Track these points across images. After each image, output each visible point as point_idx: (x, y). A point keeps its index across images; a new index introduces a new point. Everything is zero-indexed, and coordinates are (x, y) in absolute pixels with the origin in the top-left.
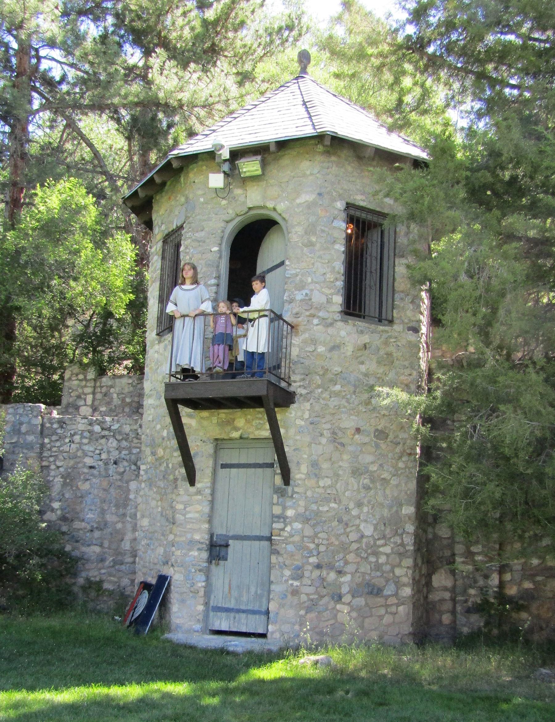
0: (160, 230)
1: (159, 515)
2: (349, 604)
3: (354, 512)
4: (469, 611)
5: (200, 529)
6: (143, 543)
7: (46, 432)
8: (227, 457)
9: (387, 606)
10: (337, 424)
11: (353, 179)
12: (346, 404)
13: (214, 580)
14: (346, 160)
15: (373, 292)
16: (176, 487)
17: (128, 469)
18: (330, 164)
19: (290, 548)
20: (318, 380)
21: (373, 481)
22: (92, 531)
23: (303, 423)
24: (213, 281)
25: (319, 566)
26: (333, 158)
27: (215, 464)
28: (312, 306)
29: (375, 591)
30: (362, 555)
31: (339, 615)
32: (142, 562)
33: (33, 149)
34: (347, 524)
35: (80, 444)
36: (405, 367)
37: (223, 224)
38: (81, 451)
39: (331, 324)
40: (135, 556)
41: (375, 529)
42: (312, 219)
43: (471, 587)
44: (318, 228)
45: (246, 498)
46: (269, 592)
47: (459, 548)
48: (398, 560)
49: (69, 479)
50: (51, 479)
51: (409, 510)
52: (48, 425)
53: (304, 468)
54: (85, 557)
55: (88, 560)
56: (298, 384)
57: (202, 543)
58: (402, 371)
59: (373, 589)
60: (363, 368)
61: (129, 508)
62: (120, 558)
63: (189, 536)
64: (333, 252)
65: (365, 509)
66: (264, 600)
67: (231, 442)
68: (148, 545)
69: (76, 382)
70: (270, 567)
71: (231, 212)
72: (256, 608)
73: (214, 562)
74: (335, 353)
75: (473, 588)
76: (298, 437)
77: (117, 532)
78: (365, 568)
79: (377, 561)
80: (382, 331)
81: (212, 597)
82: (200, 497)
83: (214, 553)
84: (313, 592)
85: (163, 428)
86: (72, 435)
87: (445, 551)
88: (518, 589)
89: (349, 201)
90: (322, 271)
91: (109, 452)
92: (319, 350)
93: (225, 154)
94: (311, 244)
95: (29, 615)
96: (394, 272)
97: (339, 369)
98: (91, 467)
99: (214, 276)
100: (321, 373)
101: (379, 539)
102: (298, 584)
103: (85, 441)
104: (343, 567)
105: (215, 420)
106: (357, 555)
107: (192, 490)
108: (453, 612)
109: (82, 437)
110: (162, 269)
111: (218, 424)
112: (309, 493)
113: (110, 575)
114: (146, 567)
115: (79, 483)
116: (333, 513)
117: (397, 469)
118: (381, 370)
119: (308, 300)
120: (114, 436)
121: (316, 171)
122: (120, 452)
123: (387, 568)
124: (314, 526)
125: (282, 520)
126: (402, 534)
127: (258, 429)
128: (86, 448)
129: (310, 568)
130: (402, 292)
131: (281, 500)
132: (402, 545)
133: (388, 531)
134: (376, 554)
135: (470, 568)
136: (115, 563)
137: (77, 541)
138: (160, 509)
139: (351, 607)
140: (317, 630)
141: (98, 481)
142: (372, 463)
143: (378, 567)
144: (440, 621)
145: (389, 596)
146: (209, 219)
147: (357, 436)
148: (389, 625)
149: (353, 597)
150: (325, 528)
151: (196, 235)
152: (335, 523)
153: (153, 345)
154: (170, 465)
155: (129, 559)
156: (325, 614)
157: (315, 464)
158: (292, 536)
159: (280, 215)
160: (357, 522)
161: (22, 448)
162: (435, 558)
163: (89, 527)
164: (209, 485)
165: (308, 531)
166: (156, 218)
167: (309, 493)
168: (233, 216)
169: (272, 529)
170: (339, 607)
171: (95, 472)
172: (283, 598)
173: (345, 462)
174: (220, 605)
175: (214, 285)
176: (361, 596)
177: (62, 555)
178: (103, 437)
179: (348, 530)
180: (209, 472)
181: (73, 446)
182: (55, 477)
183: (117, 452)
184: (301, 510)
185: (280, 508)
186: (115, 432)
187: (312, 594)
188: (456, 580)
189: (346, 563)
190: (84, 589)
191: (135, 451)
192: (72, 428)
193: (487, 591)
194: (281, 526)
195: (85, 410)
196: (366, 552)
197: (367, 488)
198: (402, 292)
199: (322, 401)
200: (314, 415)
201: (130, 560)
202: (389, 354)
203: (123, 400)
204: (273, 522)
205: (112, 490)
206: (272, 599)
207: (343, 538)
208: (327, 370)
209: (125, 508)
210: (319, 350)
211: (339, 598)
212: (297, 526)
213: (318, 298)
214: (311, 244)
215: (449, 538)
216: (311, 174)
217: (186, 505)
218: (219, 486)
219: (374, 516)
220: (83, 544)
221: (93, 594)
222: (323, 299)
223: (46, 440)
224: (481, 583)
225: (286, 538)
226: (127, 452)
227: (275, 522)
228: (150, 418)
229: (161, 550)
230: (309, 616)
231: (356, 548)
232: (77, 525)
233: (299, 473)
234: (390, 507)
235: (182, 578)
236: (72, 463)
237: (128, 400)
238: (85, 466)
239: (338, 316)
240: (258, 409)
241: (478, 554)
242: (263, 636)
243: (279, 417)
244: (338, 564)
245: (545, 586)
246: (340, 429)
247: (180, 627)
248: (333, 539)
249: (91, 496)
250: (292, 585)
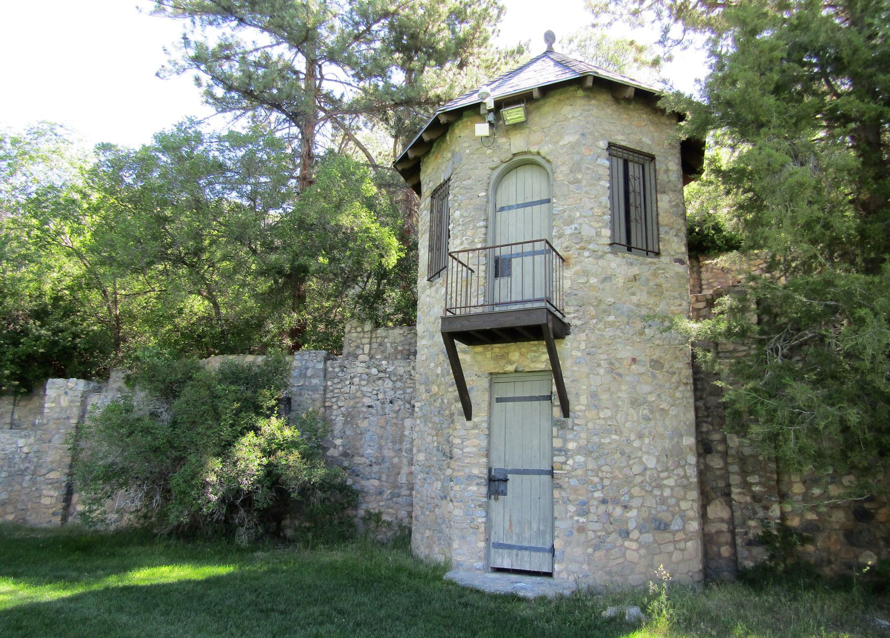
2: (637, 540)
3: (636, 444)
4: (750, 543)
5: (478, 463)
6: (419, 477)
7: (328, 376)
8: (504, 390)
9: (675, 542)
10: (613, 355)
12: (621, 335)
13: (493, 515)
15: (639, 226)
16: (453, 422)
18: (591, 107)
19: (573, 482)
23: (579, 354)
24: (482, 224)
25: (604, 502)
26: (593, 102)
27: (491, 398)
28: (582, 239)
29: (662, 526)
31: (628, 553)
34: (629, 457)
36: (675, 298)
37: (489, 171)
39: (602, 257)
40: (412, 489)
41: (658, 461)
42: (577, 158)
44: (584, 166)
46: (553, 528)
47: (735, 479)
48: (682, 493)
51: (690, 441)
53: (583, 399)
54: (365, 490)
57: (481, 478)
59: (660, 524)
60: (634, 299)
61: (404, 443)
62: (397, 491)
63: (467, 470)
64: (599, 188)
65: (647, 441)
69: (355, 334)
70: (553, 503)
71: (496, 159)
72: (540, 546)
73: (493, 497)
74: (607, 285)
76: (575, 368)
77: (393, 466)
78: (651, 502)
79: (662, 494)
80: (651, 263)
81: (493, 533)
83: (493, 488)
85: (436, 366)
86: (351, 378)
87: (719, 482)
88: (801, 520)
89: (611, 141)
90: (590, 205)
92: (591, 282)
93: (490, 105)
95: (313, 548)
98: (369, 407)
100: (595, 304)
102: (585, 520)
103: (364, 383)
104: (629, 501)
106: (642, 488)
108: (733, 544)
109: (361, 379)
110: (431, 221)
113: (388, 507)
118: (651, 301)
119: (577, 234)
120: (389, 378)
121: (577, 114)
123: (672, 501)
125: (563, 453)
126: (684, 466)
128: (364, 389)
129: (595, 503)
130: (666, 225)
131: (561, 432)
132: (685, 476)
133: (670, 463)
134: (660, 487)
136: (393, 495)
137: (358, 475)
138: (436, 444)
140: (607, 569)
141: (375, 419)
142: (650, 393)
143: (663, 501)
144: (719, 554)
145: (677, 531)
146: (476, 168)
147: (633, 367)
148: (678, 563)
149: (641, 532)
150: (608, 461)
152: (617, 456)
154: (446, 401)
155: (405, 492)
156: (613, 552)
157: (594, 395)
158: (574, 469)
159: (544, 158)
162: (708, 488)
163: (368, 462)
164: (485, 418)
165: (591, 465)
166: (424, 177)
167: (590, 425)
168: (498, 162)
169: (552, 462)
170: (627, 544)
171: (373, 411)
172: (569, 535)
173: (624, 393)
175: (483, 227)
176: (648, 532)
177: (343, 488)
178: (380, 378)
179: (631, 462)
180: (485, 405)
181: (352, 387)
182: (337, 416)
184: (583, 442)
185: (561, 440)
190: (364, 519)
192: (351, 371)
194: (561, 459)
196: (650, 485)
197: (647, 419)
198: (666, 225)
199: (596, 331)
200: (590, 345)
201: (407, 492)
202: (659, 286)
203: (396, 348)
204: (553, 455)
207: (626, 471)
210: (591, 282)
212: (580, 459)
213: (587, 231)
214: (578, 181)
215: (721, 469)
217: (463, 439)
218: (495, 419)
219: (655, 447)
220: (362, 478)
221: (373, 525)
222: (593, 233)
223: (329, 383)
224: (761, 514)
225: (569, 472)
226: (401, 392)
228: (424, 358)
229: (439, 485)
230: (597, 554)
231: (640, 481)
232: (357, 460)
233: (578, 405)
234: (672, 438)
236: (352, 403)
237: (400, 348)
238: (363, 406)
239: (607, 249)
241: (756, 484)
242: (549, 575)
245: (830, 517)
246: (617, 359)
247: (462, 565)
248: (617, 473)
249: (370, 433)
250: (577, 521)
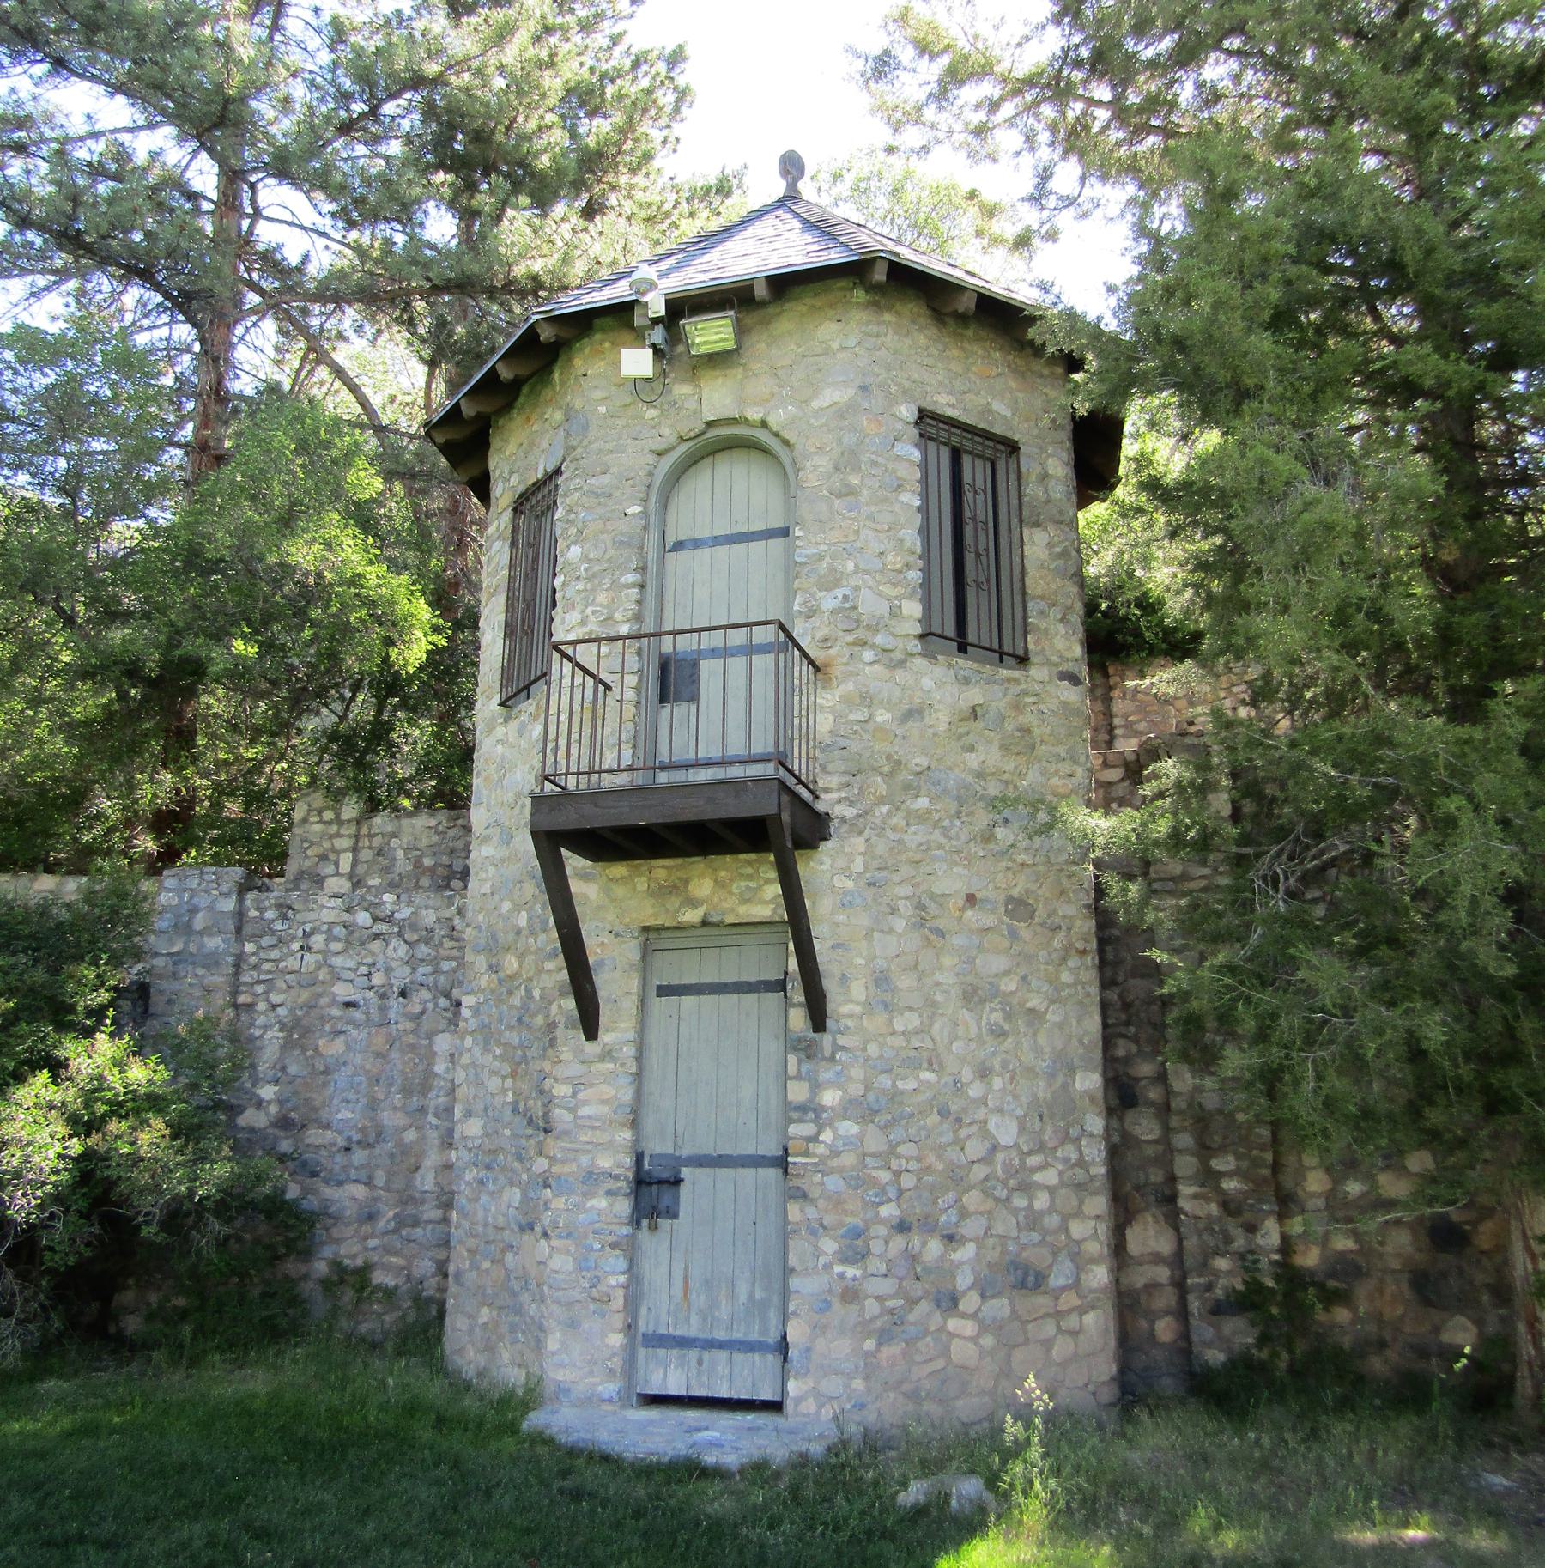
0: (504, 491)
1: (508, 1112)
2: (974, 1316)
3: (975, 1091)
4: (1217, 1310)
7: (248, 930)
8: (673, 969)
10: (924, 887)
11: (931, 361)
12: (943, 841)
13: (646, 1266)
14: (913, 322)
16: (553, 1043)
17: (430, 1006)
18: (883, 329)
19: (834, 1183)
20: (879, 785)
21: (1008, 1017)
22: (348, 1149)
23: (850, 884)
24: (631, 578)
25: (902, 1227)
26: (887, 317)
27: (644, 986)
29: (1028, 1280)
30: (997, 1193)
32: (466, 1224)
33: (243, 385)
34: (958, 1120)
35: (325, 952)
38: (325, 970)
39: (902, 663)
40: (448, 1205)
41: (1022, 1129)
42: (850, 439)
43: (1218, 1253)
44: (865, 458)
45: (715, 1066)
46: (785, 1293)
47: (1185, 1165)
49: (298, 1033)
50: (257, 1033)
51: (1090, 1081)
52: (253, 913)
53: (858, 990)
55: (337, 1218)
56: (835, 795)
57: (617, 1177)
58: (1054, 767)
59: (1026, 1274)
60: (973, 760)
61: (432, 1095)
62: (410, 1210)
63: (585, 1160)
65: (997, 1083)
66: (773, 1316)
67: (678, 933)
68: (481, 1182)
69: (318, 828)
70: (785, 1233)
71: (666, 431)
72: (754, 1336)
73: (645, 1222)
74: (913, 726)
75: (1223, 1255)
76: (841, 918)
77: (405, 1150)
78: (1005, 1225)
79: (1031, 1206)
80: (1009, 680)
81: (643, 1311)
82: (611, 1066)
84: (891, 1291)
85: (517, 908)
86: (306, 935)
90: (877, 547)
91: (388, 970)
92: (879, 719)
93: (658, 307)
94: (849, 492)
95: (194, 1362)
96: (1022, 556)
97: (924, 761)
98: (348, 1005)
99: (634, 565)
100: (886, 769)
101: (1030, 1153)
102: (858, 1273)
103: (337, 946)
104: (957, 1225)
105: (642, 884)
106: (987, 1193)
107: (592, 1048)
111: (651, 893)
112: (873, 1049)
113: (388, 1250)
114: (476, 1236)
115: (321, 1042)
116: (928, 1095)
117: (1057, 986)
119: (849, 609)
120: (400, 934)
121: (852, 342)
122: (414, 970)
123: (1052, 1221)
124: (885, 1128)
125: (811, 1115)
126: (1079, 1139)
127: (745, 901)
128: (338, 961)
129: (882, 1231)
130: (1042, 598)
132: (1081, 1163)
134: (1026, 1188)
135: (1214, 1209)
136: (401, 1222)
137: (314, 1174)
138: (510, 1097)
139: (981, 1322)
140: (906, 1387)
141: (363, 1035)
142: (1007, 973)
143: (1033, 1220)
144: (1152, 1335)
145: (1064, 1289)
147: (969, 913)
148: (1064, 1364)
149: (983, 1296)
151: (593, 481)
152: (934, 1118)
153: (489, 731)
154: (537, 993)
155: (431, 1213)
157: (881, 980)
158: (835, 1153)
159: (776, 435)
160: (981, 1114)
161: (194, 964)
162: (1128, 1187)
163: (341, 1142)
164: (631, 1035)
165: (875, 1142)
167: (873, 1049)
168: (673, 439)
170: (953, 1324)
171: (357, 1015)
174: (662, 1331)
175: (633, 585)
178: (377, 936)
179: (963, 1133)
180: (630, 1004)
181: (308, 957)
182: (265, 1028)
183: (407, 970)
184: (856, 1090)
186: (402, 925)
187: (892, 1297)
188: (1180, 1241)
189: (964, 1214)
190: (327, 1285)
191: (446, 966)
192: (305, 918)
193: (1256, 1262)
194: (807, 1129)
195: (336, 884)
198: (1042, 598)
200: (875, 864)
201: (436, 1214)
202: (1026, 731)
204: (788, 1121)
205: (395, 1055)
206: (795, 1313)
207: (952, 1154)
208: (899, 763)
209: (425, 1095)
210: (879, 719)
211: (949, 1302)
212: (849, 1128)
213: (871, 605)
214: (849, 492)
215: (1156, 1142)
216: (843, 348)
217: (578, 1085)
218: (653, 1037)
219: (1016, 1097)
221: (348, 1296)
222: (883, 609)
223: (249, 947)
224: (1240, 1242)
225: (823, 1160)
226: (429, 969)
227: (792, 1121)
228: (486, 888)
232: (314, 1136)
233: (844, 1004)
235: (570, 1267)
236: (305, 995)
238: (333, 1002)
239: (915, 646)
240: (742, 856)
241: (1230, 1175)
242: (775, 1406)
243: (802, 870)
244: (944, 1218)
246: (933, 897)
248: (931, 1158)
249: (349, 1070)
250: (842, 1276)
